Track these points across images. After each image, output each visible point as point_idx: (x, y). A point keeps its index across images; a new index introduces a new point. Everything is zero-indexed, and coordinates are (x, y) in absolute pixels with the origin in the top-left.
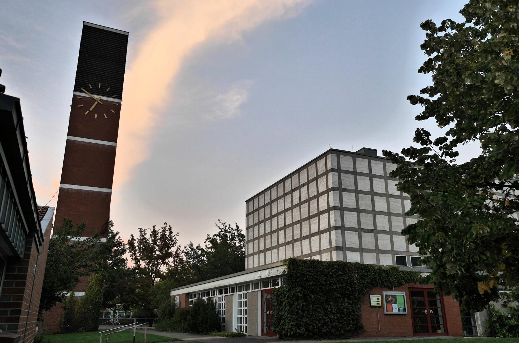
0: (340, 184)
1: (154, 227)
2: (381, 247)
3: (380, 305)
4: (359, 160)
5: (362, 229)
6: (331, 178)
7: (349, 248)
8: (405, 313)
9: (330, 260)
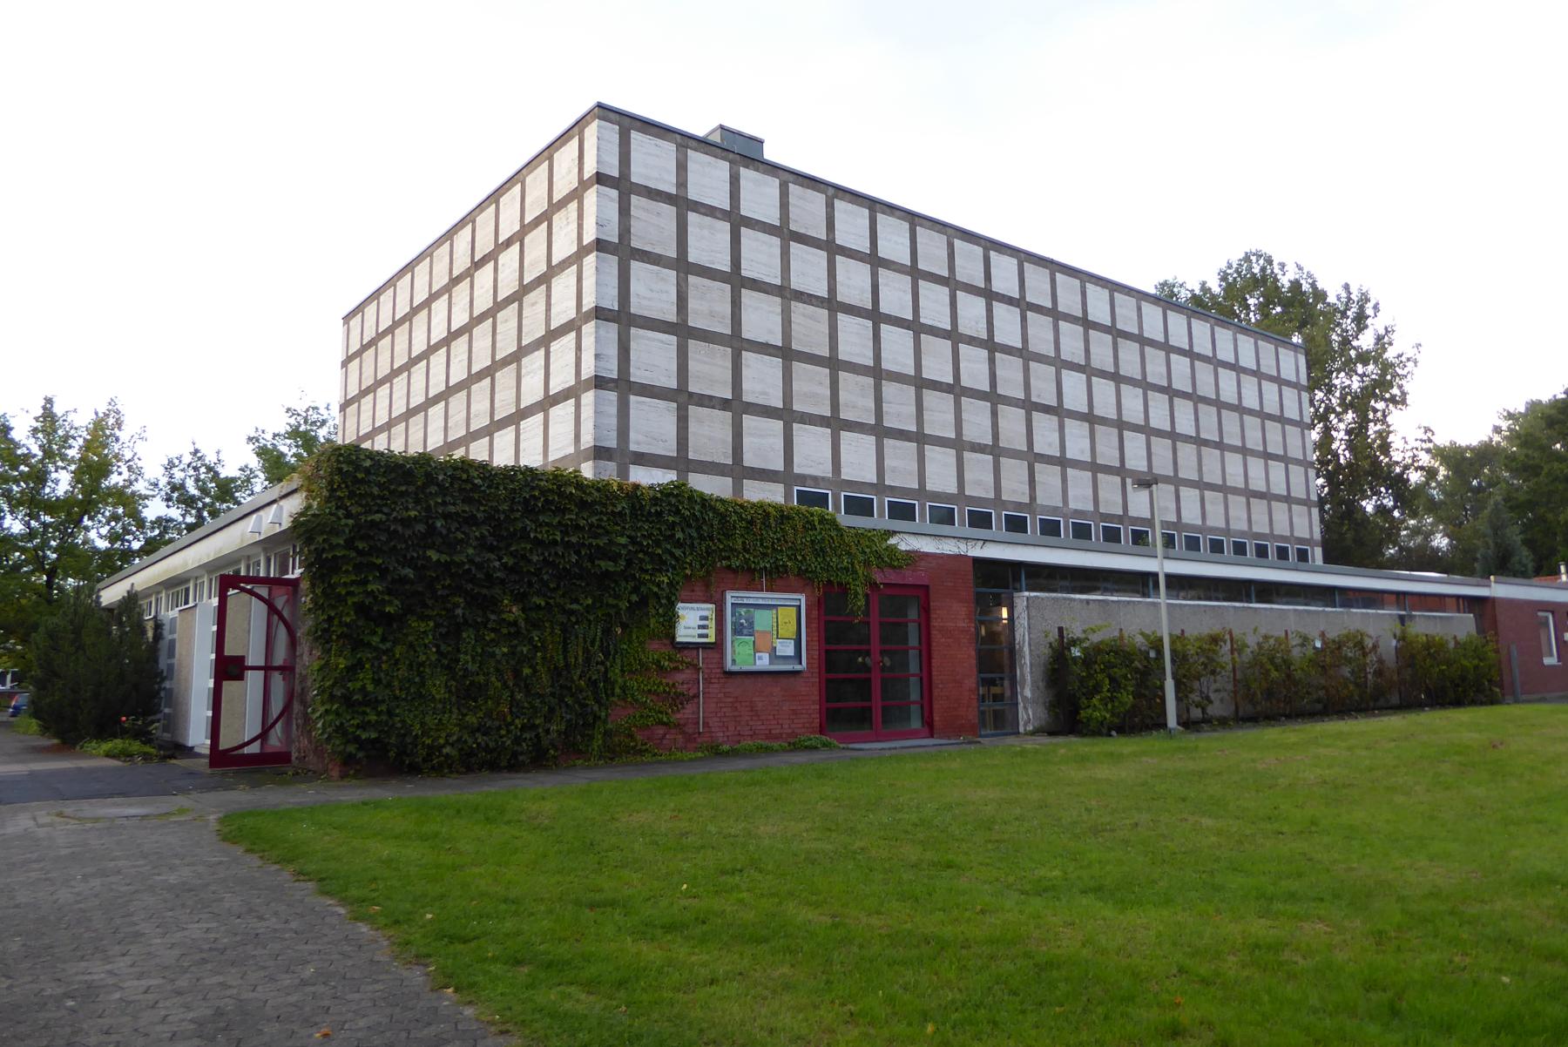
0: (625, 231)
1: (49, 401)
2: (749, 460)
3: (712, 639)
4: (698, 161)
5: (691, 394)
6: (594, 209)
7: (643, 454)
8: (798, 667)
9: (511, 463)
